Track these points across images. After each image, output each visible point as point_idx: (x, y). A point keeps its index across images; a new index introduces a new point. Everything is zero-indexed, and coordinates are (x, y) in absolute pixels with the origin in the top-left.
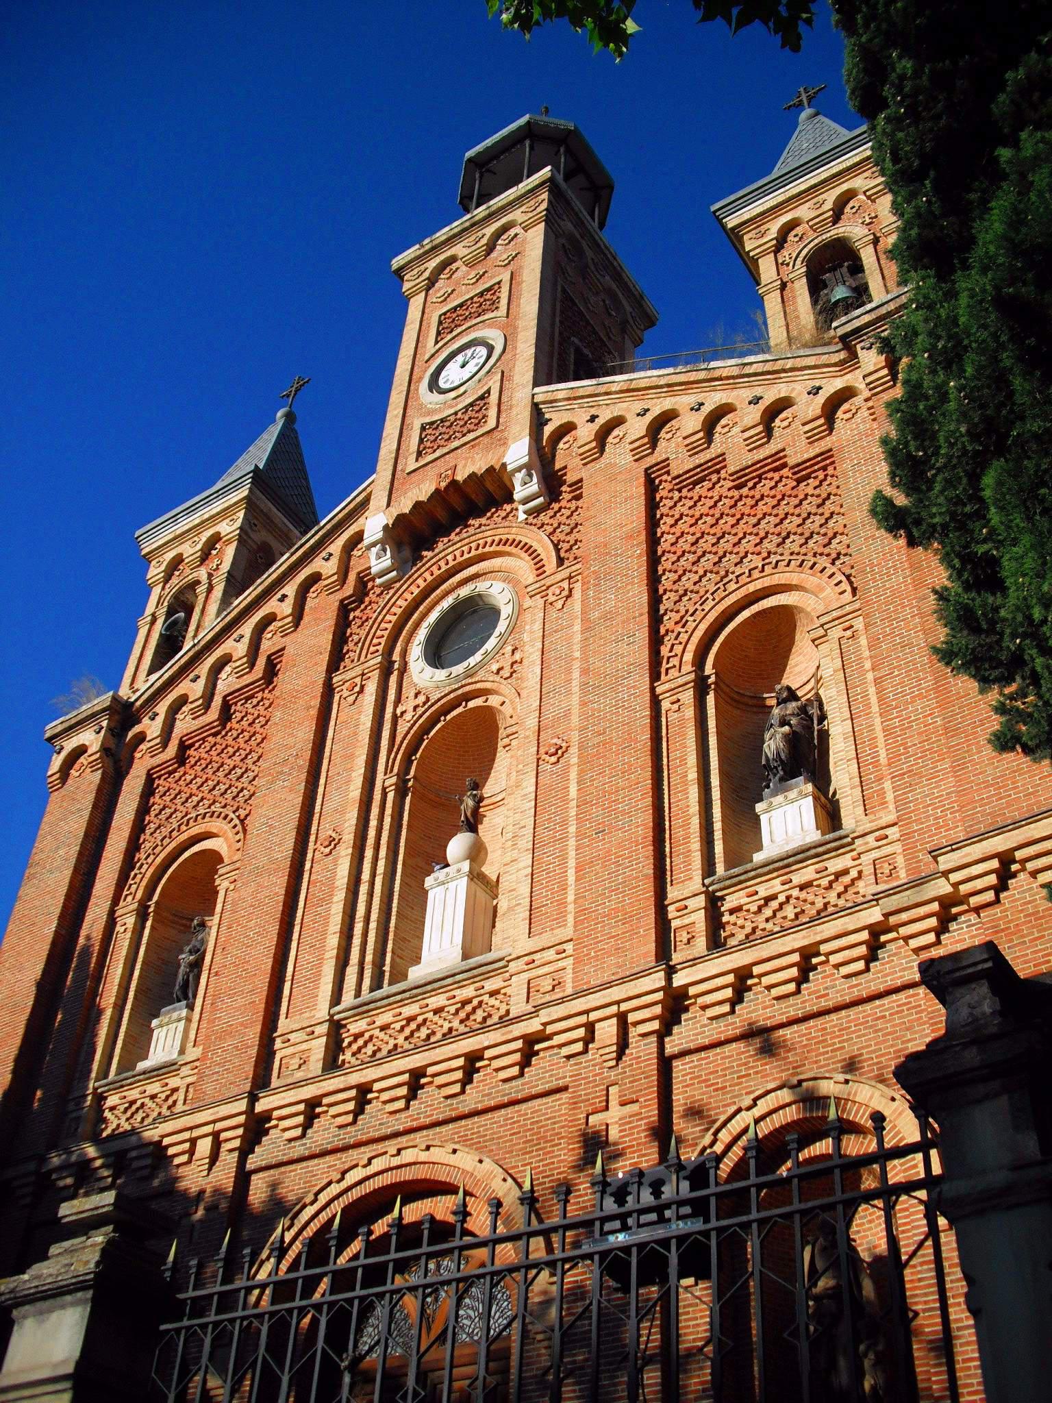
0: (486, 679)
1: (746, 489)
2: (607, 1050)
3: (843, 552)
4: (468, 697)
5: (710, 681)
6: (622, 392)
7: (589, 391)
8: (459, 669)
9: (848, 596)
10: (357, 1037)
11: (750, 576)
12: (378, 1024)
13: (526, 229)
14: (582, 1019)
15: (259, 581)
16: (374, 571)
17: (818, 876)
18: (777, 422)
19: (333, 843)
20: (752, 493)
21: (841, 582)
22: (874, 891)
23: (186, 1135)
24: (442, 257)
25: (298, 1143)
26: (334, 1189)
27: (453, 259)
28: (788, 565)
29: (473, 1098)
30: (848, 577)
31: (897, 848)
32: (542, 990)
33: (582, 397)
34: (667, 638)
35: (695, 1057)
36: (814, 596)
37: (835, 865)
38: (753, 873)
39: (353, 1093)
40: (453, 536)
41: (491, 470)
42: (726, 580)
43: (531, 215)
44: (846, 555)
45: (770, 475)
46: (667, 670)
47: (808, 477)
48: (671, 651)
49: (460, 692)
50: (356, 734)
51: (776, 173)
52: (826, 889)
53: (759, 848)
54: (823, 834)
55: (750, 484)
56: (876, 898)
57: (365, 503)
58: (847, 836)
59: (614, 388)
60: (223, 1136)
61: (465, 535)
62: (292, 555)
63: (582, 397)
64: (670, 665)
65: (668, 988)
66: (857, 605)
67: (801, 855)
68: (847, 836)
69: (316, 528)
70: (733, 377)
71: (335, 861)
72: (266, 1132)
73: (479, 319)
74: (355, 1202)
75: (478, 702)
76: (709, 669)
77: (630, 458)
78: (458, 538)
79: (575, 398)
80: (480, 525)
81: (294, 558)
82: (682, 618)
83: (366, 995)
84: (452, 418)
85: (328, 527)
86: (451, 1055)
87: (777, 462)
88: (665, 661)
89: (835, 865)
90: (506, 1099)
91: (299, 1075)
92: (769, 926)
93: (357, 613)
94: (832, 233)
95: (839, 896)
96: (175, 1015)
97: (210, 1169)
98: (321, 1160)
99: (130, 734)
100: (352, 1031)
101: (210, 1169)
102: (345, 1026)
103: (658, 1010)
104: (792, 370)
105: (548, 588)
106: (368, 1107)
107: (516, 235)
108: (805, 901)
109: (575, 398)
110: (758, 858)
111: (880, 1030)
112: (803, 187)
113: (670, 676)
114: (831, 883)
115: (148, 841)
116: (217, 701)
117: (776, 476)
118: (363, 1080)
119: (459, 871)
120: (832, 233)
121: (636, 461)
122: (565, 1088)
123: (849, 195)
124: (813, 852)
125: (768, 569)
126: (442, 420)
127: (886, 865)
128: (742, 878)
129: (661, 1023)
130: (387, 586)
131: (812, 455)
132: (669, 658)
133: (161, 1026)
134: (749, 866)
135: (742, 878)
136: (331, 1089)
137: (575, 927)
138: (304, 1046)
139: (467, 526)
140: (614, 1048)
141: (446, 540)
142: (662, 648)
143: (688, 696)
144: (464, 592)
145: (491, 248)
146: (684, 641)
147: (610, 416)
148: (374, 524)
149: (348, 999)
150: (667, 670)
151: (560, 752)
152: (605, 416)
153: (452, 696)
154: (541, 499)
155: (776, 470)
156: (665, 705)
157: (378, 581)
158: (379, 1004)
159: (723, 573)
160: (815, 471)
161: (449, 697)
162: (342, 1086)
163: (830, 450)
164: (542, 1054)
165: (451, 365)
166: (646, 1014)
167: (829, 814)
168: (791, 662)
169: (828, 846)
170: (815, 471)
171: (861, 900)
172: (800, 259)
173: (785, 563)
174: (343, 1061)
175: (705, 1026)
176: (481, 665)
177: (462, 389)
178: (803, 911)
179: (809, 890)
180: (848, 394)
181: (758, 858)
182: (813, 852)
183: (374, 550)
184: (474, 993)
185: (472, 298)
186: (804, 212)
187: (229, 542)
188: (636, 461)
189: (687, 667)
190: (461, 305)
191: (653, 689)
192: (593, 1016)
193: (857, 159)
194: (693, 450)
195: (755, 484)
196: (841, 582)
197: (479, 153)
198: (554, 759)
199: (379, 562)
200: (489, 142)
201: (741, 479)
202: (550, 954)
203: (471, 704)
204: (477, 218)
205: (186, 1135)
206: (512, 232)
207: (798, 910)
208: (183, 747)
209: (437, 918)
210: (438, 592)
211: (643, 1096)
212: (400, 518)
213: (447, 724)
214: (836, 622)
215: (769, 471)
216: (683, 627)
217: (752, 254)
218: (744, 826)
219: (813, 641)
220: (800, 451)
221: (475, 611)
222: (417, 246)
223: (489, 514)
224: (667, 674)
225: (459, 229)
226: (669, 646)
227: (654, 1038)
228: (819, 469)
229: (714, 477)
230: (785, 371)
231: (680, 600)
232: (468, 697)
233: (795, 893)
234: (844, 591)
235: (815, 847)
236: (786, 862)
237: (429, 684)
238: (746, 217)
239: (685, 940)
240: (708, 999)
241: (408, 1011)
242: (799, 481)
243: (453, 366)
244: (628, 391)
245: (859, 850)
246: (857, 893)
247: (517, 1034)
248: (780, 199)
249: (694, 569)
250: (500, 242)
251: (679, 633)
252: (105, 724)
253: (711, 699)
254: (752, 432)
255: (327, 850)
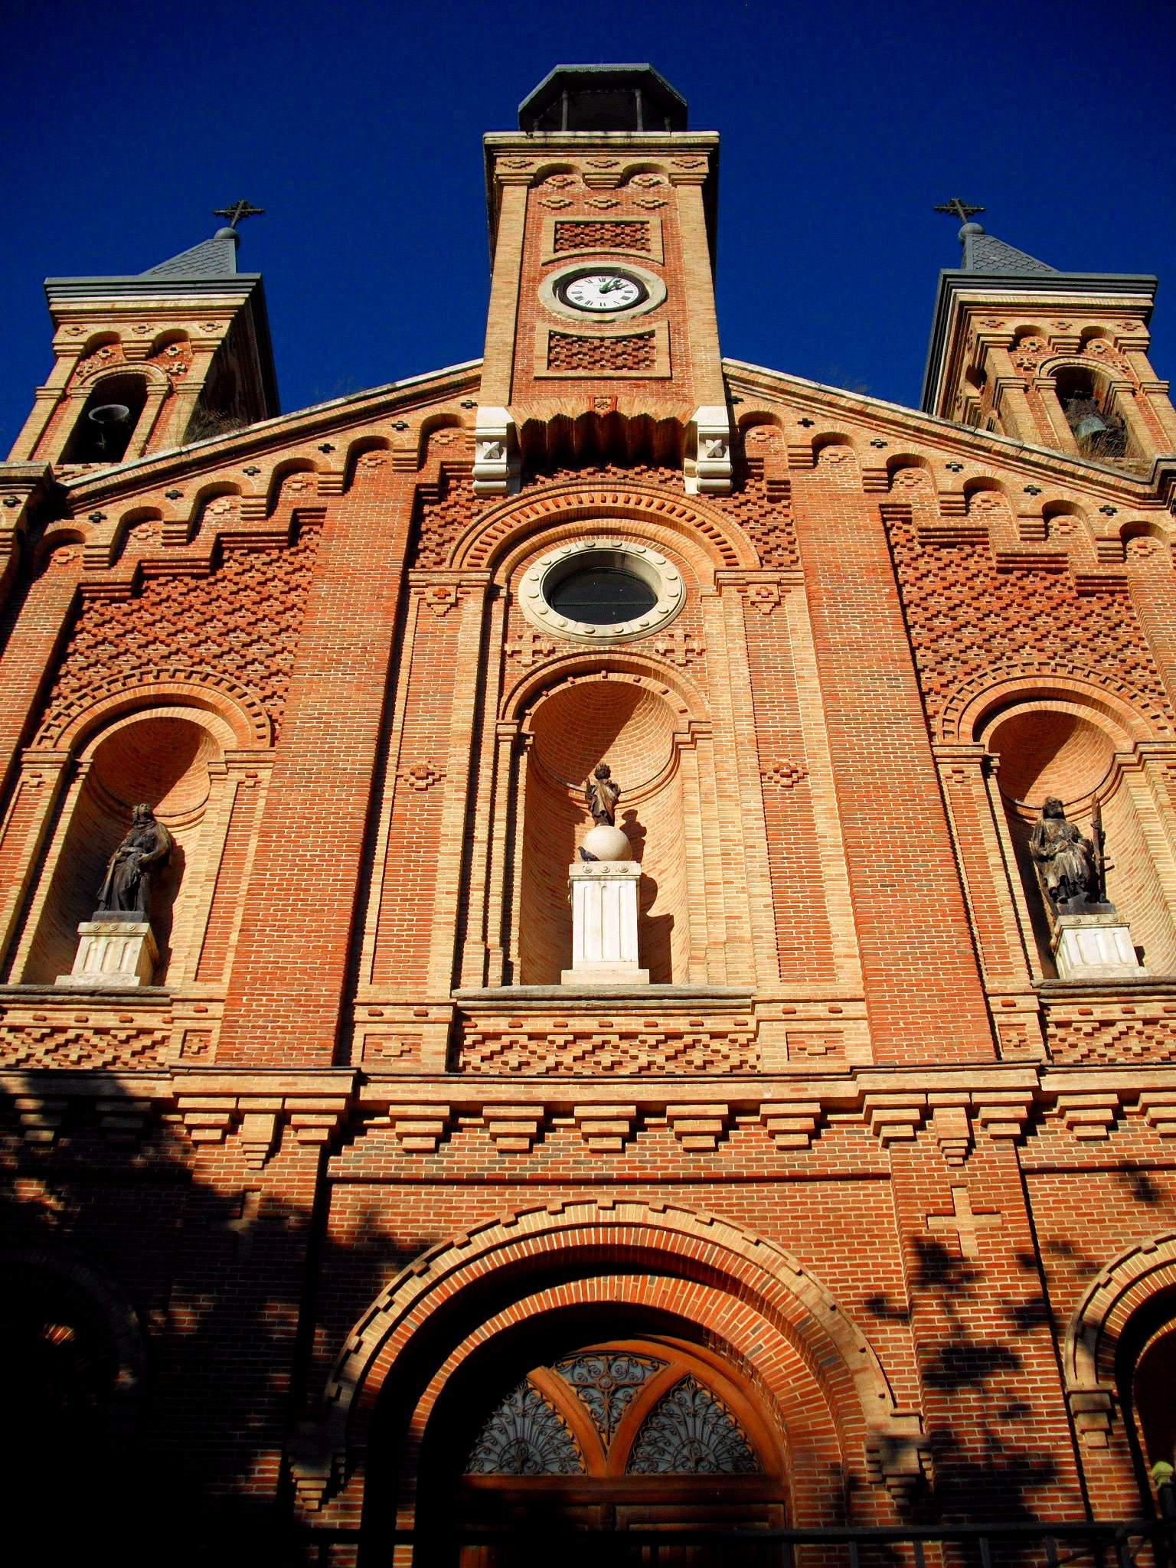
0: (646, 652)
1: (205, 582)
2: (954, 1143)
3: (279, 693)
4: (611, 667)
5: (81, 770)
6: (851, 410)
7: (806, 392)
8: (602, 630)
9: (267, 741)
10: (487, 1037)
11: (157, 677)
12: (527, 1029)
13: (674, 183)
14: (920, 1099)
15: (294, 414)
16: (476, 469)
17: (36, 1023)
18: (135, 531)
19: (431, 778)
20: (159, 589)
21: (263, 725)
22: (173, 1063)
23: (230, 1103)
24: (555, 161)
25: (425, 1158)
26: (500, 1234)
27: (567, 169)
28: (217, 684)
29: (729, 1159)
30: (273, 721)
31: (216, 1026)
32: (810, 1050)
33: (794, 394)
34: (55, 703)
35: (1056, 1178)
36: (225, 729)
37: (143, 1020)
38: (1090, 990)
39: (632, 1109)
40: (583, 473)
41: (672, 423)
42: (144, 669)
43: (598, 170)
44: (281, 697)
45: (187, 579)
46: (42, 738)
47: (1092, 594)
48: (56, 718)
49: (606, 657)
50: (451, 653)
51: (145, 276)
52: (121, 1042)
53: (68, 972)
54: (142, 983)
55: (162, 580)
56: (173, 1072)
57: (473, 383)
58: (167, 996)
59: (842, 402)
60: (984, 1113)
61: (600, 479)
62: (350, 402)
63: (794, 394)
64: (48, 734)
65: (352, 1097)
66: (272, 756)
67: (101, 998)
68: (167, 996)
69: (388, 386)
70: (1006, 456)
71: (437, 800)
72: (363, 1131)
73: (613, 250)
74: (524, 1261)
75: (628, 678)
76: (87, 756)
77: (859, 484)
78: (590, 479)
79: (783, 392)
80: (625, 477)
81: (353, 408)
82: (82, 687)
83: (496, 987)
84: (597, 343)
85: (407, 392)
86: (709, 1098)
87: (1055, 565)
88: (43, 727)
89: (143, 1020)
90: (787, 1172)
91: (402, 1066)
92: (134, 1062)
93: (436, 508)
94: (138, 367)
95: (47, 1052)
96: (127, 926)
97: (266, 1161)
98: (466, 1190)
99: (51, 528)
100: (480, 1029)
101: (266, 1161)
102: (468, 1018)
103: (332, 1120)
104: (1083, 478)
105: (748, 584)
106: (549, 1135)
107: (658, 183)
108: (94, 1046)
109: (783, 392)
110: (62, 981)
111: (401, 1214)
112: (1050, 301)
113: (41, 747)
114: (129, 1037)
115: (507, 679)
116: (206, 535)
117: (193, 583)
118: (560, 1098)
119: (625, 870)
120: (138, 367)
121: (866, 491)
122: (886, 1177)
123: (111, 339)
124: (1164, 988)
125: (164, 676)
126: (580, 338)
127: (196, 1040)
128: (1077, 991)
129: (330, 1135)
130: (486, 495)
131: (1104, 574)
132: (50, 725)
133: (97, 934)
134: (47, 988)
135: (1077, 991)
136: (504, 1097)
137: (230, 988)
138: (408, 1028)
139: (656, 471)
140: (266, 1148)
141: (573, 474)
142: (47, 711)
143: (51, 776)
144: (603, 543)
145: (624, 180)
146: (74, 714)
147: (831, 430)
148: (492, 417)
149: (471, 985)
150: (42, 738)
151: (795, 776)
152: (824, 426)
153: (593, 657)
154: (504, 484)
155: (1049, 571)
156: (25, 776)
157: (476, 484)
158: (534, 1004)
159: (145, 660)
160: (1102, 592)
161: (587, 658)
162: (523, 1098)
163: (1125, 578)
164: (835, 1128)
165: (595, 280)
166: (211, 1119)
167: (157, 963)
168: (1041, 778)
169: (1098, 990)
170: (1102, 592)
171: (154, 1066)
172: (92, 379)
173: (215, 680)
174: (466, 1063)
175: (678, 1155)
176: (638, 636)
177: (608, 317)
178: (89, 1056)
179: (19, 1035)
180: (1142, 529)
181: (62, 981)
182: (1164, 988)
183: (488, 446)
184: (690, 1029)
185: (603, 223)
186: (127, 331)
187: (200, 349)
188: (866, 491)
189: (66, 743)
190: (587, 224)
191: (405, 575)
192: (933, 1098)
193: (1113, 303)
194: (948, 510)
195: (1024, 576)
196: (263, 725)
197: (576, 73)
198: (786, 781)
199: (488, 462)
200: (593, 68)
201: (1008, 564)
202: (821, 1010)
203: (614, 677)
204: (612, 141)
205: (230, 1103)
206: (656, 178)
207: (85, 1053)
208: (141, 576)
209: (592, 920)
210: (560, 528)
211: (1007, 1208)
212: (532, 425)
213: (575, 688)
214: (1159, 756)
215: (1042, 569)
216: (79, 699)
217: (56, 348)
218: (59, 945)
219: (210, 774)
220: (1086, 561)
221: (605, 571)
222: (524, 134)
223: (637, 469)
224: (39, 743)
225: (586, 141)
226: (55, 712)
227: (317, 1150)
228: (1106, 592)
229: (968, 549)
230: (1073, 475)
231: (87, 668)
232: (611, 667)
233: (88, 1034)
234: (264, 737)
235: (82, 994)
236: (1132, 989)
237: (554, 632)
238: (981, 299)
239: (195, 1048)
240: (1083, 1115)
241: (578, 1024)
242: (1082, 594)
243: (597, 282)
244: (861, 413)
245: (174, 1014)
246: (154, 1059)
247: (817, 1094)
248: (1023, 300)
249: (272, 640)
250: (550, 180)
251: (72, 704)
252: (24, 498)
253: (76, 788)
254: (1031, 522)
255: (422, 784)
